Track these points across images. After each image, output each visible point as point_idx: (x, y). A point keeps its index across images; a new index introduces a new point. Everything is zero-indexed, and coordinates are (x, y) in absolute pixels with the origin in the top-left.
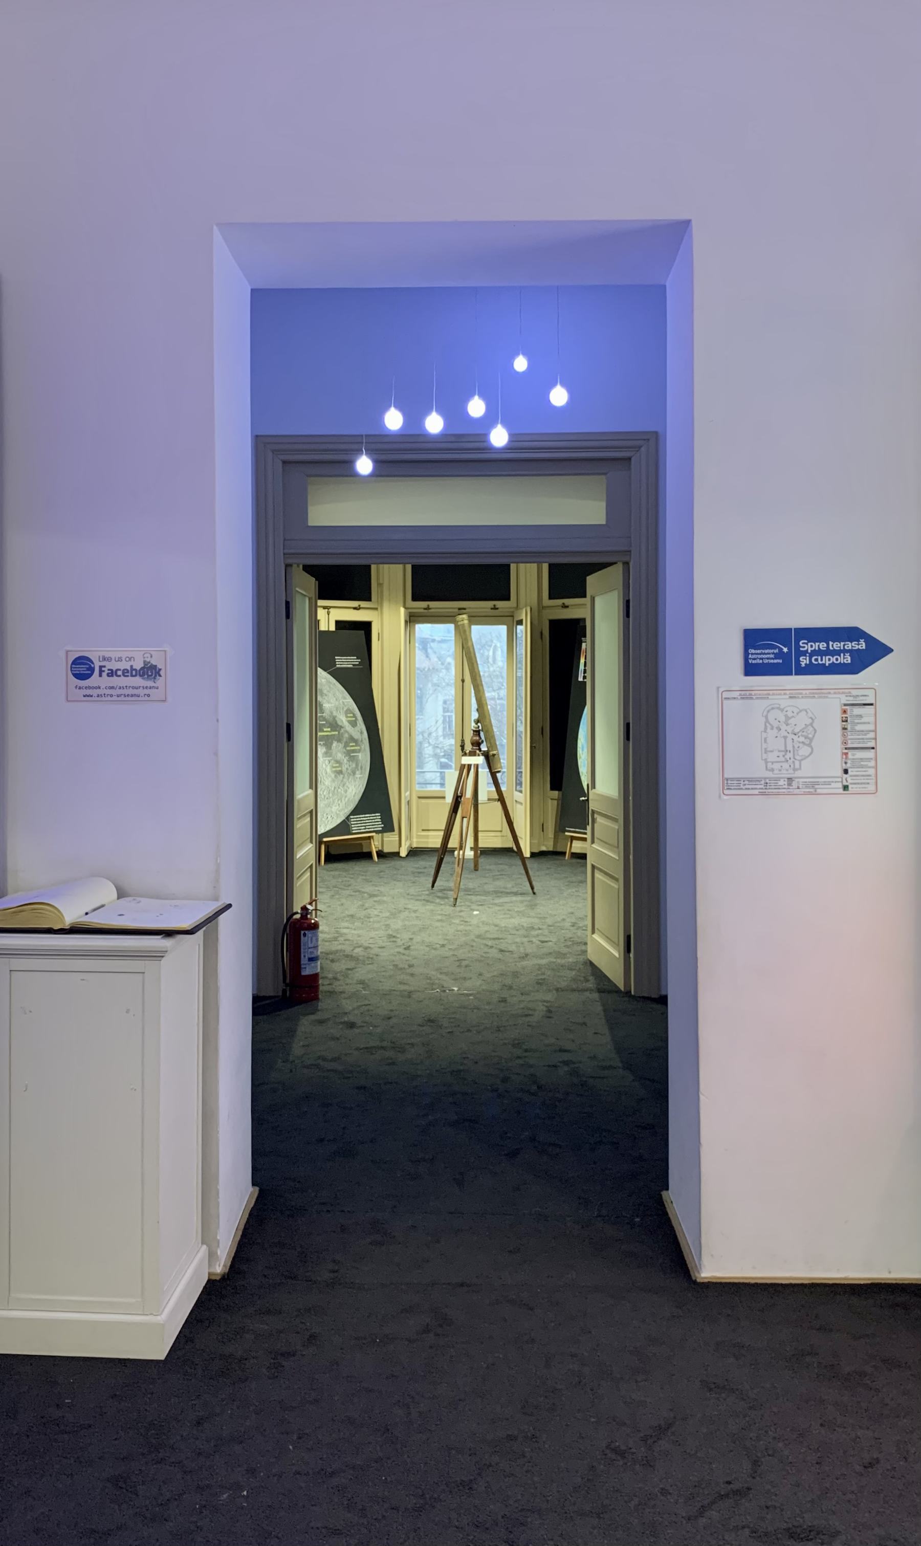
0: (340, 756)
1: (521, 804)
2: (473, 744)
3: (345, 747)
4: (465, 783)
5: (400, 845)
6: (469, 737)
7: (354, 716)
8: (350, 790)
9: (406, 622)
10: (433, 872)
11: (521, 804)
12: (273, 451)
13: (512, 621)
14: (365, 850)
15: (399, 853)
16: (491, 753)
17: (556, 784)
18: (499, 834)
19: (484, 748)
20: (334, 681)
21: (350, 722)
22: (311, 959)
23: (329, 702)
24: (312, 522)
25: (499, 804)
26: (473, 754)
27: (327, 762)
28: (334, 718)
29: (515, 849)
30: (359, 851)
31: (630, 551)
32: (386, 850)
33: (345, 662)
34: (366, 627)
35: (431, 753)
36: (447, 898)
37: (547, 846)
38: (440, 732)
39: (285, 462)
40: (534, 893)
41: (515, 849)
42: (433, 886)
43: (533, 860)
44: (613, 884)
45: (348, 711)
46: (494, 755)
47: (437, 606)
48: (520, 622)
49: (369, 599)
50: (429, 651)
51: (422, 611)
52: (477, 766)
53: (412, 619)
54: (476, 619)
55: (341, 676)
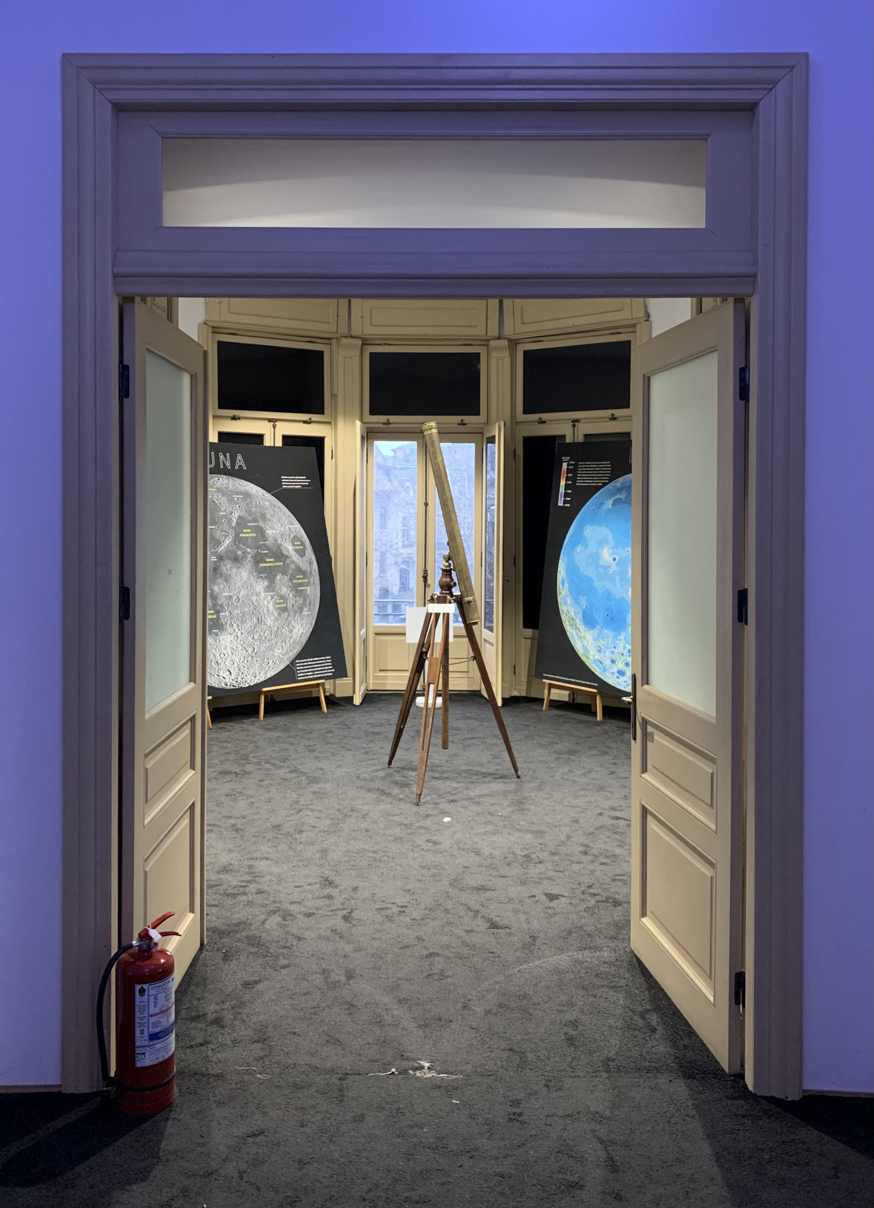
0: (284, 590)
1: (492, 645)
2: (442, 587)
3: (291, 580)
4: (432, 633)
5: (354, 692)
6: (436, 578)
7: (303, 544)
8: (296, 630)
9: (362, 438)
10: (392, 735)
11: (492, 645)
12: (94, 83)
13: (483, 439)
14: (314, 695)
15: (352, 698)
16: (466, 599)
17: (531, 619)
18: (464, 675)
19: (456, 592)
20: (280, 504)
21: (296, 551)
22: (154, 1037)
23: (273, 529)
24: (170, 221)
25: (474, 664)
26: (442, 600)
27: (269, 598)
28: (279, 546)
29: (485, 693)
30: (309, 696)
31: (755, 276)
32: (338, 695)
33: (294, 482)
34: (318, 443)
35: (393, 562)
36: (408, 785)
37: (520, 691)
38: (400, 545)
39: (119, 108)
40: (518, 777)
41: (485, 693)
42: (390, 763)
43: (505, 708)
44: (703, 869)
45: (296, 539)
46: (469, 602)
47: (396, 420)
48: (491, 440)
49: (320, 411)
50: (392, 477)
51: (382, 426)
52: (447, 616)
53: (370, 435)
54: (446, 435)
55: (287, 498)
